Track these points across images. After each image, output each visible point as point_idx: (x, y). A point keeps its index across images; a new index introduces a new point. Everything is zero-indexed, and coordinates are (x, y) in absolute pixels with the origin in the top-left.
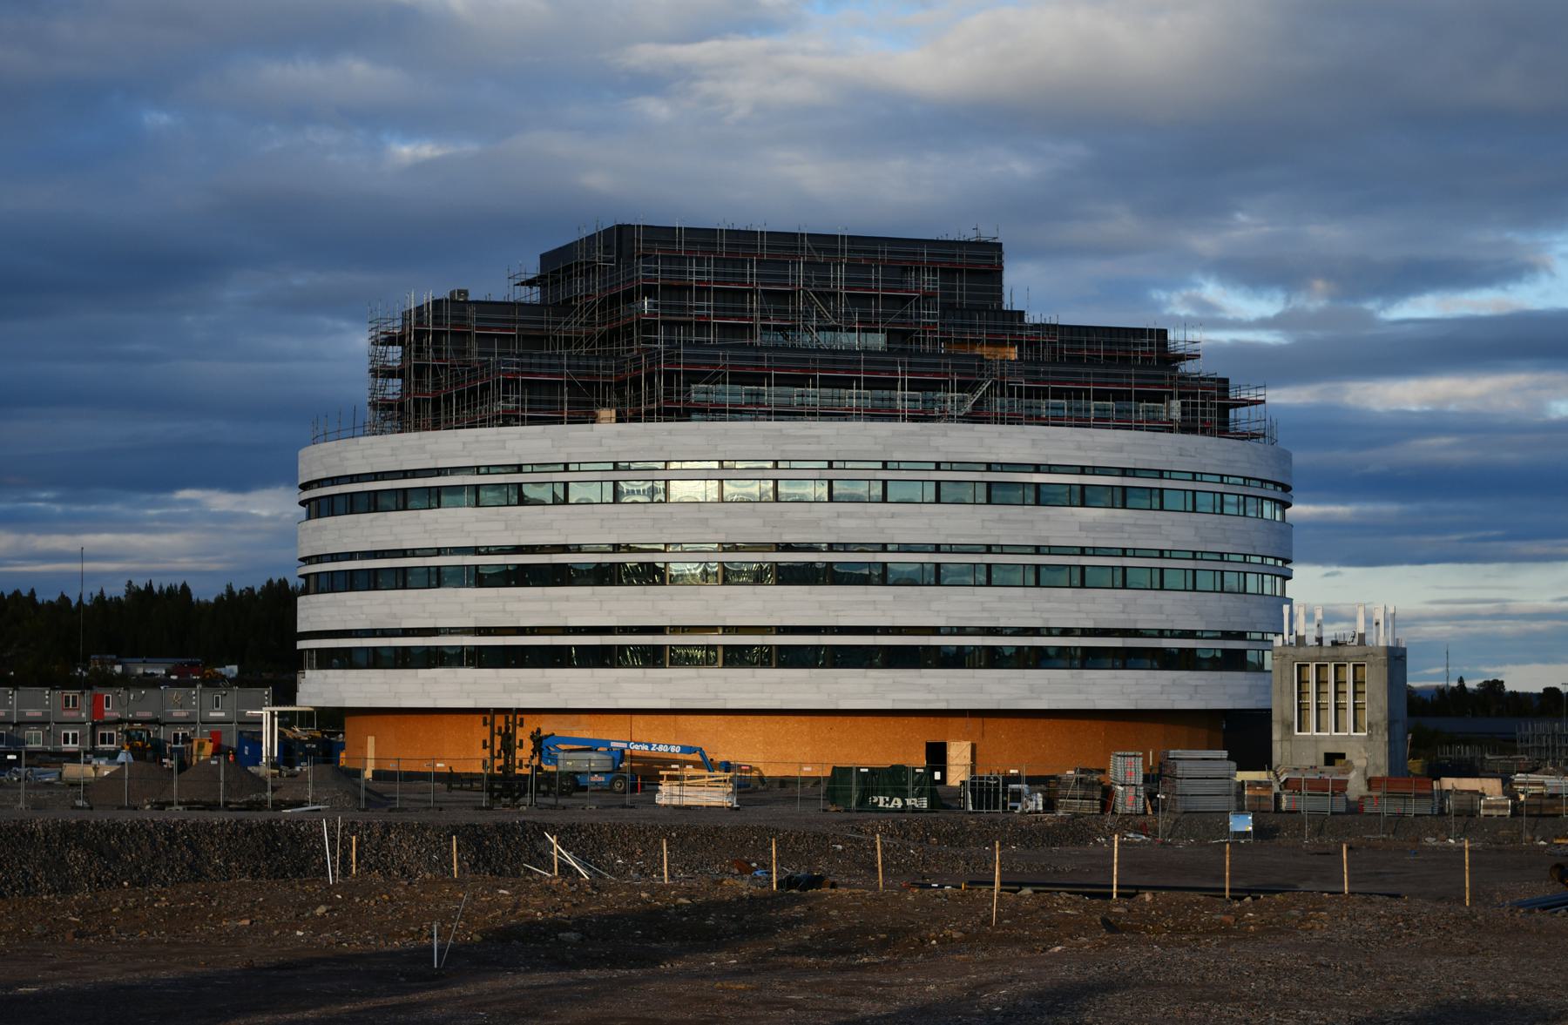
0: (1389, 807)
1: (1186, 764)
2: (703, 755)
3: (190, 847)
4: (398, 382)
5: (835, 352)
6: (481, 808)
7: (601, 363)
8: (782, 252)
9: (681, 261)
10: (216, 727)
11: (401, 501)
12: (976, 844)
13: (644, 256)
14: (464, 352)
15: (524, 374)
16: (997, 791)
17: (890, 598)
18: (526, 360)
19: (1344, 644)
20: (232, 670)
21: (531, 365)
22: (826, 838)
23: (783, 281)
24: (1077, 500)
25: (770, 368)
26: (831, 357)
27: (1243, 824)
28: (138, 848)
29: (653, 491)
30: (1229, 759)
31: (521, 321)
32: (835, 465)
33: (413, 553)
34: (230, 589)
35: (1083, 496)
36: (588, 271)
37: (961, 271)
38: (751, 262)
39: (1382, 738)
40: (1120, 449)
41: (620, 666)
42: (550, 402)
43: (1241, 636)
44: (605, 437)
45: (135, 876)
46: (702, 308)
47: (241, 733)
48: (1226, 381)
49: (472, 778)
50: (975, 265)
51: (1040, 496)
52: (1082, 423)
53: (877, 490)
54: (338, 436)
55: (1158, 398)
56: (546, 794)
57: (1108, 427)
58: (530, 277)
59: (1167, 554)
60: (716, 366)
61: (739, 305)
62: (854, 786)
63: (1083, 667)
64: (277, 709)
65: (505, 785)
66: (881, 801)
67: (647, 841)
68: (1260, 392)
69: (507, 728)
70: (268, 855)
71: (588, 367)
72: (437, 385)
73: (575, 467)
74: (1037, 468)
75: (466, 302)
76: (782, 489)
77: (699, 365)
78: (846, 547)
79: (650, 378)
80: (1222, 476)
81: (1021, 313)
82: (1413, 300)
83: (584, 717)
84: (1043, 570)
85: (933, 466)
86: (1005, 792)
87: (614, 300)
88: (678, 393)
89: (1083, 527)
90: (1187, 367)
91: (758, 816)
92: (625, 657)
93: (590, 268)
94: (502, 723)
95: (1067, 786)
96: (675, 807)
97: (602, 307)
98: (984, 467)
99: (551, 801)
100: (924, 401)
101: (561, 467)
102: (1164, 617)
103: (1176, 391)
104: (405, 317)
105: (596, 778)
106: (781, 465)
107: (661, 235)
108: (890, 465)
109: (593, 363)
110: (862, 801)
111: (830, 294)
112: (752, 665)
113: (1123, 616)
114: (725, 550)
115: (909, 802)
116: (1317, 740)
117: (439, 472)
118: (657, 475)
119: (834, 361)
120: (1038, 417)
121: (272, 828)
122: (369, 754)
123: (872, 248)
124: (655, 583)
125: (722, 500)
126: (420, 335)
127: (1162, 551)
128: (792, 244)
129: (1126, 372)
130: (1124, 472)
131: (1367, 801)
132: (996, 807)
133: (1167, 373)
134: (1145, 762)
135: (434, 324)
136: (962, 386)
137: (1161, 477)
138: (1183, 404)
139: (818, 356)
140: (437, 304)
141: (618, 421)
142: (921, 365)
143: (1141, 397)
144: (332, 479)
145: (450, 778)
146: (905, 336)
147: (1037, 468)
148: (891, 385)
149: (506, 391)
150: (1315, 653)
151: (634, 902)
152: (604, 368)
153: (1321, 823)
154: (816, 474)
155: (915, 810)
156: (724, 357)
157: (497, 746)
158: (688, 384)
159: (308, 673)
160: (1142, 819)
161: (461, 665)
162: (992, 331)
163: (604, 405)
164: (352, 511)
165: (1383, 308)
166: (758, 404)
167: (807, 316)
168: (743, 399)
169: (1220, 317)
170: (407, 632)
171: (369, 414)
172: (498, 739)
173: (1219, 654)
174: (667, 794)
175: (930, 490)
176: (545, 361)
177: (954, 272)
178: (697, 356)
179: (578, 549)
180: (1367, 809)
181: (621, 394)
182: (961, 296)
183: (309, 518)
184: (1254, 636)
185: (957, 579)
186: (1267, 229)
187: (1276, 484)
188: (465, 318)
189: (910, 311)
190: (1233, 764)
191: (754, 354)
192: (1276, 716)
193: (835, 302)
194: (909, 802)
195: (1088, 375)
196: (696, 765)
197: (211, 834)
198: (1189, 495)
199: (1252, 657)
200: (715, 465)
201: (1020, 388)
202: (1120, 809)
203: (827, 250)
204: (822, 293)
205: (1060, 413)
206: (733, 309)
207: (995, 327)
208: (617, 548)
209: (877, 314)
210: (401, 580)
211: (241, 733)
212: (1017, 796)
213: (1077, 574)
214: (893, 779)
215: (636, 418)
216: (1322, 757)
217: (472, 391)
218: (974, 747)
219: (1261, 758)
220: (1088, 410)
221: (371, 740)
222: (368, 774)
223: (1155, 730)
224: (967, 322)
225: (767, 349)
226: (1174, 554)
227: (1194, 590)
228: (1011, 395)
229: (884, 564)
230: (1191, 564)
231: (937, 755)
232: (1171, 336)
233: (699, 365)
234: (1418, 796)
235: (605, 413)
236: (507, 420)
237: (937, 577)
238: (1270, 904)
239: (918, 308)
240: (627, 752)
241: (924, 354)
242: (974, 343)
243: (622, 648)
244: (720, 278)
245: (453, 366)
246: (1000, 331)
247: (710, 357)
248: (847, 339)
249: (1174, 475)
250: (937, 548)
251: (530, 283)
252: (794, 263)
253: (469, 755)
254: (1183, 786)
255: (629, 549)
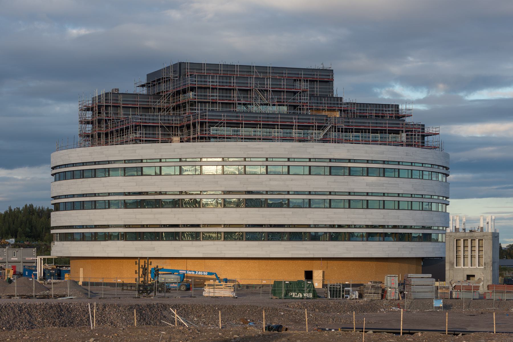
0: (495, 297)
1: (415, 279)
2: (216, 276)
3: (28, 313)
4: (90, 126)
5: (268, 114)
6: (136, 298)
7: (174, 118)
8: (245, 73)
9: (205, 77)
10: (14, 264)
11: (93, 174)
12: (334, 312)
13: (190, 75)
14: (117, 114)
15: (143, 122)
16: (340, 291)
17: (291, 213)
18: (144, 117)
19: (474, 231)
20: (12, 241)
21: (145, 119)
22: (276, 310)
23: (246, 85)
24: (365, 174)
25: (242, 120)
26: (267, 116)
27: (439, 303)
28: (8, 314)
29: (196, 170)
30: (432, 277)
31: (140, 101)
32: (269, 159)
33: (99, 195)
34: (10, 210)
35: (368, 172)
36: (167, 81)
37: (317, 81)
38: (234, 77)
39: (490, 269)
40: (382, 153)
41: (182, 240)
42: (153, 134)
43: (430, 228)
44: (176, 148)
45: (8, 325)
46: (214, 96)
47: (24, 266)
48: (423, 125)
49: (131, 285)
50: (323, 78)
51: (351, 172)
52: (367, 143)
53: (285, 169)
54: (67, 148)
55: (397, 132)
56: (160, 292)
57: (377, 144)
58: (143, 83)
59: (401, 195)
60: (221, 119)
61: (229, 95)
62: (283, 289)
63: (367, 240)
64: (42, 257)
65: (144, 289)
66: (294, 294)
67: (206, 311)
68: (437, 129)
69: (145, 266)
70: (59, 317)
71: (168, 120)
72: (107, 127)
73: (164, 160)
74: (350, 161)
75: (118, 93)
76: (248, 169)
77: (360, 126)
78: (272, 193)
79: (194, 125)
80: (423, 164)
81: (341, 98)
82: (478, 92)
83: (167, 261)
84: (351, 202)
85: (308, 160)
86: (343, 291)
87: (178, 93)
88: (206, 130)
89: (367, 184)
90: (408, 120)
91: (248, 300)
92: (184, 237)
93: (168, 80)
94: (143, 263)
95: (368, 289)
96: (212, 297)
97: (173, 96)
98: (328, 161)
99: (163, 294)
100: (304, 134)
101: (159, 160)
102: (399, 220)
103: (404, 129)
104: (93, 99)
105: (174, 285)
106: (247, 160)
107: (197, 67)
108: (291, 160)
109: (170, 118)
110: (286, 295)
111: (265, 90)
112: (235, 240)
113: (383, 220)
114: (224, 194)
115: (305, 295)
116: (464, 270)
117: (109, 162)
118: (197, 163)
119: (268, 118)
120: (350, 141)
121: (59, 306)
122: (82, 275)
123: (281, 72)
124: (196, 207)
125: (223, 173)
126: (100, 107)
127: (367, 193)
128: (249, 70)
129: (383, 122)
130: (384, 162)
131: (487, 294)
132: (339, 297)
133: (401, 122)
134: (399, 279)
135: (106, 103)
136: (319, 128)
137: (399, 164)
138: (407, 135)
139: (262, 115)
140: (107, 94)
141: (181, 142)
142: (303, 119)
143: (390, 132)
144: (59, 166)
145: (123, 285)
146: (295, 107)
147: (350, 161)
148: (291, 127)
149: (136, 130)
150: (463, 235)
151: (217, 337)
152: (175, 120)
153: (469, 303)
154: (261, 163)
155: (307, 298)
156: (224, 116)
157: (141, 273)
158: (209, 127)
159: (56, 243)
160: (398, 302)
161: (118, 240)
162: (330, 105)
163: (175, 135)
164: (73, 178)
165: (466, 95)
166: (237, 135)
167: (256, 99)
168: (231, 133)
169: (411, 99)
170: (96, 227)
171: (79, 139)
172: (141, 270)
173: (421, 235)
174: (208, 292)
175: (307, 170)
176: (152, 118)
177: (314, 81)
178: (213, 116)
179: (165, 193)
180: (487, 298)
181: (182, 131)
182: (317, 91)
183: (55, 181)
184: (435, 228)
185: (317, 206)
186: (420, 64)
187: (443, 167)
188: (117, 100)
189: (297, 97)
190: (434, 280)
191: (236, 115)
192: (447, 260)
193: (267, 94)
194: (305, 295)
195: (369, 123)
196: (214, 280)
197: (36, 308)
198: (410, 171)
199: (434, 236)
200: (221, 160)
201: (342, 129)
202: (389, 298)
203: (263, 73)
204: (262, 90)
205: (357, 138)
206: (226, 97)
207: (317, 103)
208: (181, 193)
209: (284, 99)
210: (94, 205)
211: (24, 266)
212: (348, 292)
213: (365, 203)
214: (297, 286)
215: (188, 141)
216: (466, 276)
217: (122, 130)
218: (324, 272)
219: (440, 276)
220: (369, 137)
221: (81, 270)
222: (80, 283)
223: (405, 266)
224: (319, 102)
225: (241, 113)
226: (404, 195)
227: (412, 209)
228: (339, 131)
229: (288, 199)
230: (410, 199)
231: (309, 275)
232: (400, 107)
233: (214, 119)
234: (507, 292)
235: (176, 139)
236: (136, 141)
237: (310, 204)
238: (470, 337)
239: (300, 96)
240: (186, 275)
241: (303, 115)
242: (323, 110)
243: (183, 233)
244: (221, 84)
245: (111, 120)
246: (332, 105)
247: (218, 116)
248: (270, 109)
249: (404, 164)
250: (310, 193)
251: (143, 86)
252: (250, 78)
253: (129, 275)
254: (414, 289)
255: (186, 193)
